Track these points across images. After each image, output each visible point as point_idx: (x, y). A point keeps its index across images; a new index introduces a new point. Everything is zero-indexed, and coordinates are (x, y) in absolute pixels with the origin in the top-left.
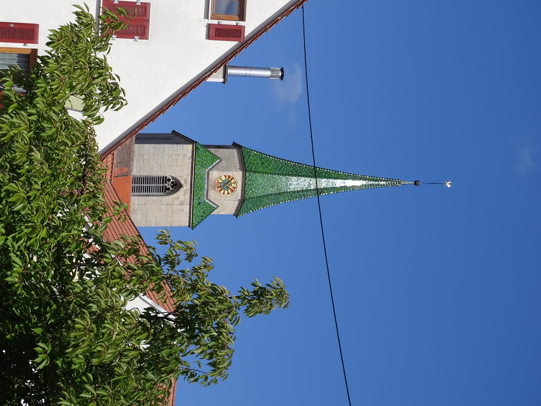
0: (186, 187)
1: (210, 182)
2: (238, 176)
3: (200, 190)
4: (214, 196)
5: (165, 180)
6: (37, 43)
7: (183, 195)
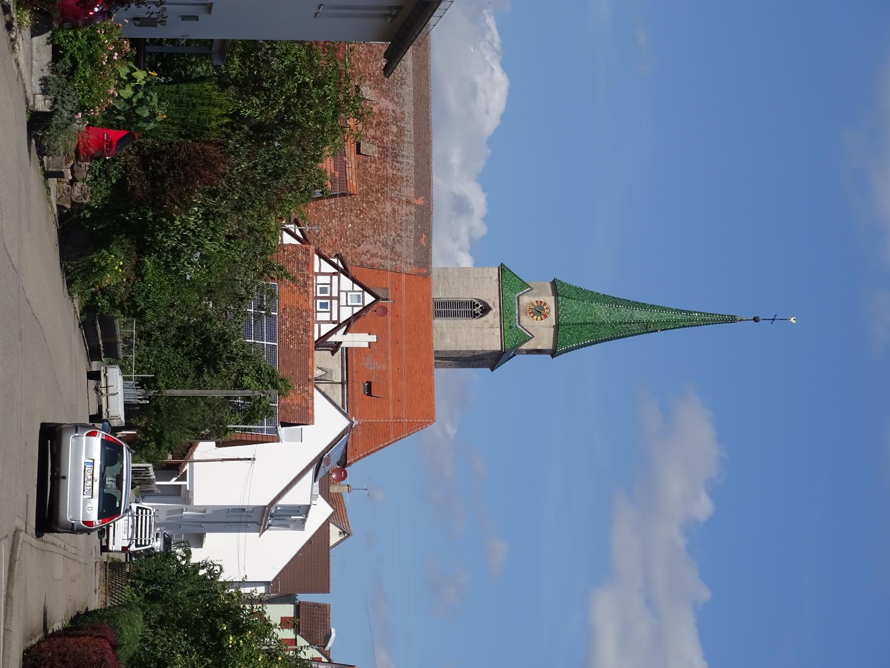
0: (495, 310)
1: (521, 308)
2: (550, 301)
3: (511, 314)
4: (527, 321)
5: (473, 305)
6: (326, 590)
7: (493, 317)
